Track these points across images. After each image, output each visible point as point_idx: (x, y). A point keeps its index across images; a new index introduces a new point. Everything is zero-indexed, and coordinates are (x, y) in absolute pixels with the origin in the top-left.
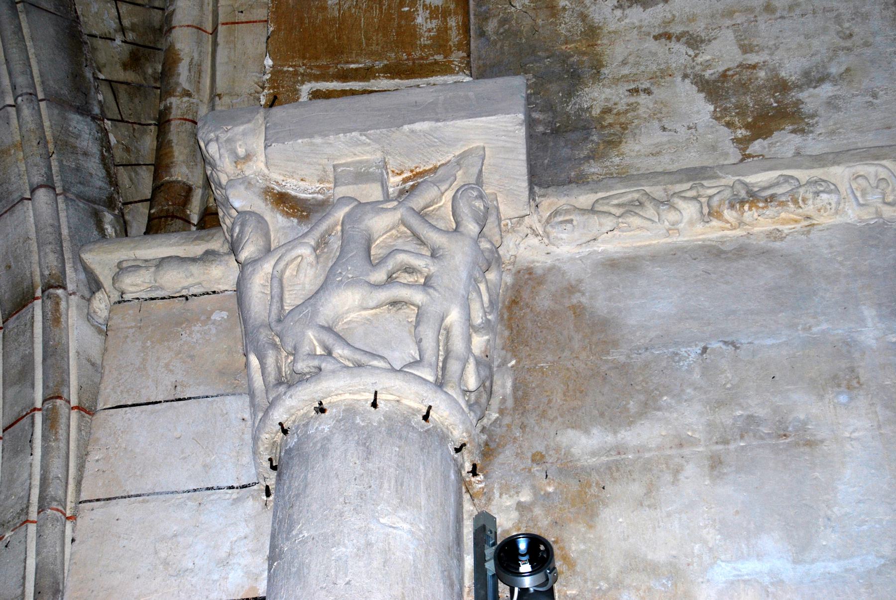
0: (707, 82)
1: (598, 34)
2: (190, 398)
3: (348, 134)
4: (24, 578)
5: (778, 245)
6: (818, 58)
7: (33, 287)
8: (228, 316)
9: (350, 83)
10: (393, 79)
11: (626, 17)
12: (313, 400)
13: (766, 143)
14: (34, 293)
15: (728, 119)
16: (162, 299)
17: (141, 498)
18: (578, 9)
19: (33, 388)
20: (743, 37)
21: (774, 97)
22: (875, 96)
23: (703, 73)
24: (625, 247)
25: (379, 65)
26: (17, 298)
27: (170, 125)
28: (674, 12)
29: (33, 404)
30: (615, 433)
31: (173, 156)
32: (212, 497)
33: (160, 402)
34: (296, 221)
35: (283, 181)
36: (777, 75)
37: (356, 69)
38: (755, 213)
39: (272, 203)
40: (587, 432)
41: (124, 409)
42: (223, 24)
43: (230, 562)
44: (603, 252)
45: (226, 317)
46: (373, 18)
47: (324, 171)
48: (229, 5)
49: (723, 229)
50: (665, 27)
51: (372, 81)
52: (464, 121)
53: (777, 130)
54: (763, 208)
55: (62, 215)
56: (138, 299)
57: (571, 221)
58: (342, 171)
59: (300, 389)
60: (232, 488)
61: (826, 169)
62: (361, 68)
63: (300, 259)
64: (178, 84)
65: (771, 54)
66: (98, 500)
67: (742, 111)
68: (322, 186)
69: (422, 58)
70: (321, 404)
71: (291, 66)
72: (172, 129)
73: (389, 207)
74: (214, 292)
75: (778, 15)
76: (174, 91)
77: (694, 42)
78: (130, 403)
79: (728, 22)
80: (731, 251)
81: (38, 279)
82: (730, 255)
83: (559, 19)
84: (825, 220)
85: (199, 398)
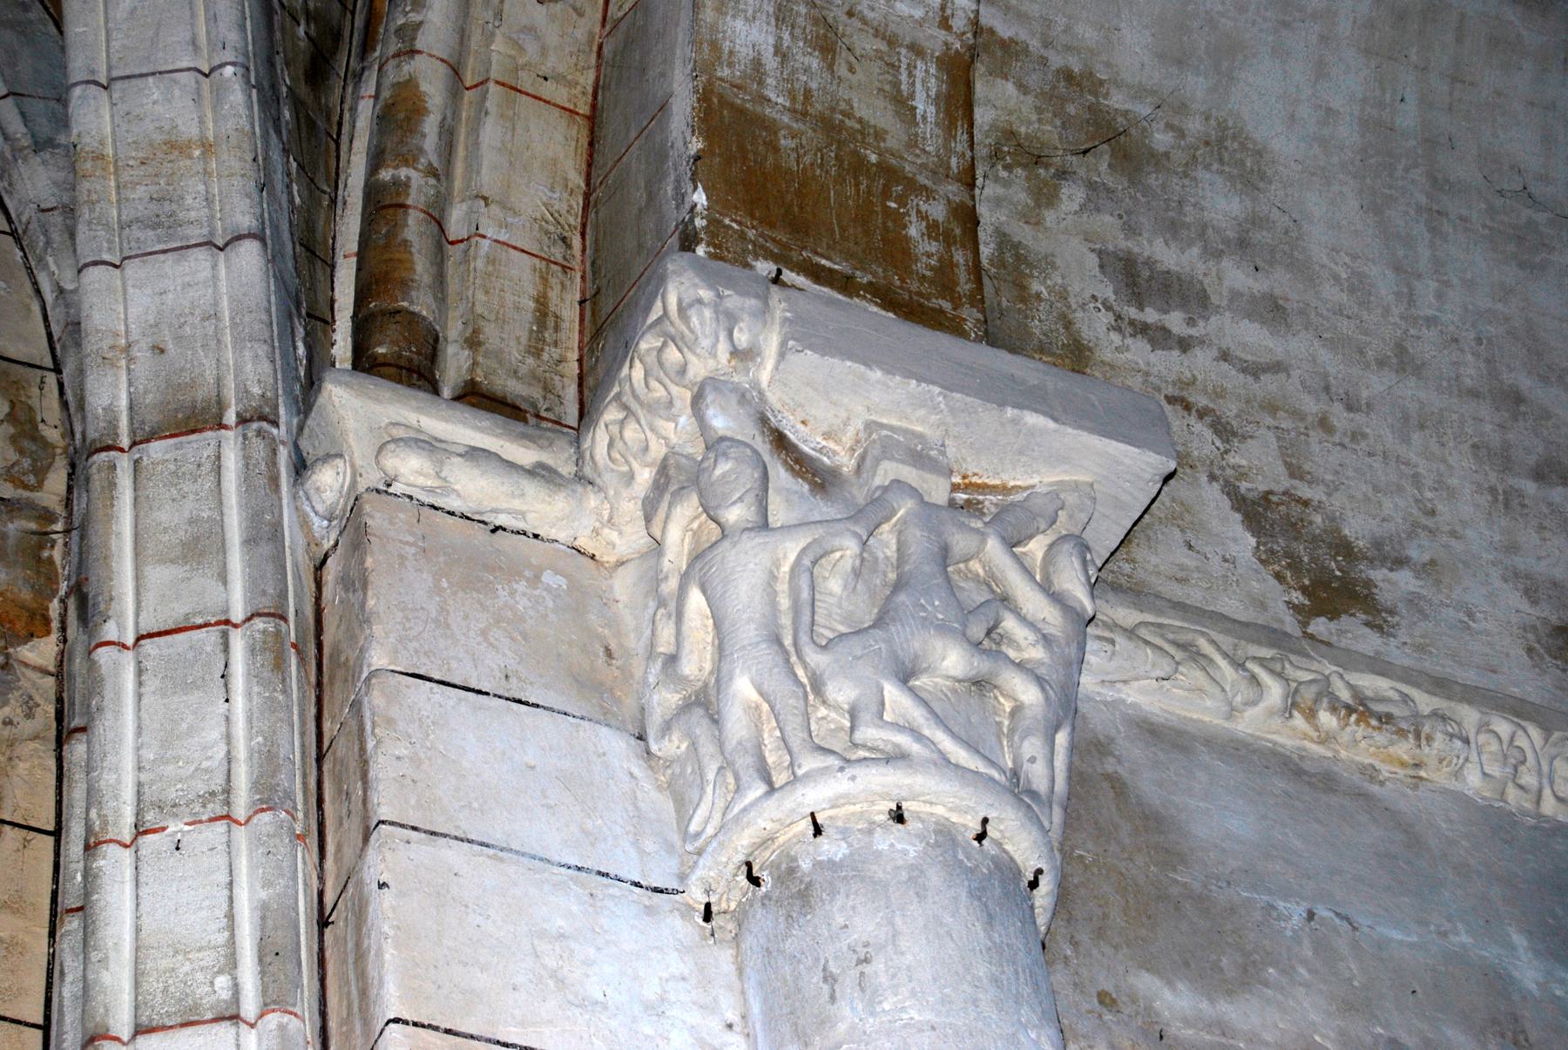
0: (1244, 499)
1: (1088, 358)
3: (923, 385)
4: (231, 916)
5: (1375, 789)
6: (1390, 527)
7: (221, 406)
11: (1128, 349)
12: (885, 796)
13: (1333, 625)
14: (221, 416)
15: (1277, 568)
16: (449, 513)
17: (491, 851)
18: (1059, 305)
19: (225, 583)
20: (1289, 452)
21: (1336, 561)
22: (1471, 615)
23: (1238, 484)
24: (1166, 711)
25: (863, 278)
27: (406, 214)
28: (1195, 372)
29: (226, 611)
30: (1212, 1001)
32: (611, 891)
33: (487, 694)
34: (806, 487)
36: (1338, 530)
37: (831, 270)
38: (1361, 731)
39: (771, 442)
40: (1170, 984)
42: (497, 82)
43: (668, 1013)
44: (1133, 705)
46: (847, 198)
48: (510, 56)
49: (1305, 736)
50: (1182, 389)
52: (1093, 437)
53: (1346, 612)
54: (1374, 728)
56: (411, 497)
57: (1113, 642)
59: (874, 771)
60: (637, 885)
61: (1453, 704)
62: (836, 271)
64: (421, 150)
65: (1329, 495)
66: (414, 828)
67: (1295, 565)
68: (824, 443)
69: (919, 294)
70: (899, 808)
71: (736, 221)
73: (972, 525)
74: (536, 536)
75: (1337, 439)
76: (415, 160)
77: (1223, 430)
78: (437, 677)
79: (1269, 421)
80: (1314, 775)
81: (230, 394)
82: (1314, 780)
83: (1031, 310)
84: (1439, 777)
85: (552, 710)
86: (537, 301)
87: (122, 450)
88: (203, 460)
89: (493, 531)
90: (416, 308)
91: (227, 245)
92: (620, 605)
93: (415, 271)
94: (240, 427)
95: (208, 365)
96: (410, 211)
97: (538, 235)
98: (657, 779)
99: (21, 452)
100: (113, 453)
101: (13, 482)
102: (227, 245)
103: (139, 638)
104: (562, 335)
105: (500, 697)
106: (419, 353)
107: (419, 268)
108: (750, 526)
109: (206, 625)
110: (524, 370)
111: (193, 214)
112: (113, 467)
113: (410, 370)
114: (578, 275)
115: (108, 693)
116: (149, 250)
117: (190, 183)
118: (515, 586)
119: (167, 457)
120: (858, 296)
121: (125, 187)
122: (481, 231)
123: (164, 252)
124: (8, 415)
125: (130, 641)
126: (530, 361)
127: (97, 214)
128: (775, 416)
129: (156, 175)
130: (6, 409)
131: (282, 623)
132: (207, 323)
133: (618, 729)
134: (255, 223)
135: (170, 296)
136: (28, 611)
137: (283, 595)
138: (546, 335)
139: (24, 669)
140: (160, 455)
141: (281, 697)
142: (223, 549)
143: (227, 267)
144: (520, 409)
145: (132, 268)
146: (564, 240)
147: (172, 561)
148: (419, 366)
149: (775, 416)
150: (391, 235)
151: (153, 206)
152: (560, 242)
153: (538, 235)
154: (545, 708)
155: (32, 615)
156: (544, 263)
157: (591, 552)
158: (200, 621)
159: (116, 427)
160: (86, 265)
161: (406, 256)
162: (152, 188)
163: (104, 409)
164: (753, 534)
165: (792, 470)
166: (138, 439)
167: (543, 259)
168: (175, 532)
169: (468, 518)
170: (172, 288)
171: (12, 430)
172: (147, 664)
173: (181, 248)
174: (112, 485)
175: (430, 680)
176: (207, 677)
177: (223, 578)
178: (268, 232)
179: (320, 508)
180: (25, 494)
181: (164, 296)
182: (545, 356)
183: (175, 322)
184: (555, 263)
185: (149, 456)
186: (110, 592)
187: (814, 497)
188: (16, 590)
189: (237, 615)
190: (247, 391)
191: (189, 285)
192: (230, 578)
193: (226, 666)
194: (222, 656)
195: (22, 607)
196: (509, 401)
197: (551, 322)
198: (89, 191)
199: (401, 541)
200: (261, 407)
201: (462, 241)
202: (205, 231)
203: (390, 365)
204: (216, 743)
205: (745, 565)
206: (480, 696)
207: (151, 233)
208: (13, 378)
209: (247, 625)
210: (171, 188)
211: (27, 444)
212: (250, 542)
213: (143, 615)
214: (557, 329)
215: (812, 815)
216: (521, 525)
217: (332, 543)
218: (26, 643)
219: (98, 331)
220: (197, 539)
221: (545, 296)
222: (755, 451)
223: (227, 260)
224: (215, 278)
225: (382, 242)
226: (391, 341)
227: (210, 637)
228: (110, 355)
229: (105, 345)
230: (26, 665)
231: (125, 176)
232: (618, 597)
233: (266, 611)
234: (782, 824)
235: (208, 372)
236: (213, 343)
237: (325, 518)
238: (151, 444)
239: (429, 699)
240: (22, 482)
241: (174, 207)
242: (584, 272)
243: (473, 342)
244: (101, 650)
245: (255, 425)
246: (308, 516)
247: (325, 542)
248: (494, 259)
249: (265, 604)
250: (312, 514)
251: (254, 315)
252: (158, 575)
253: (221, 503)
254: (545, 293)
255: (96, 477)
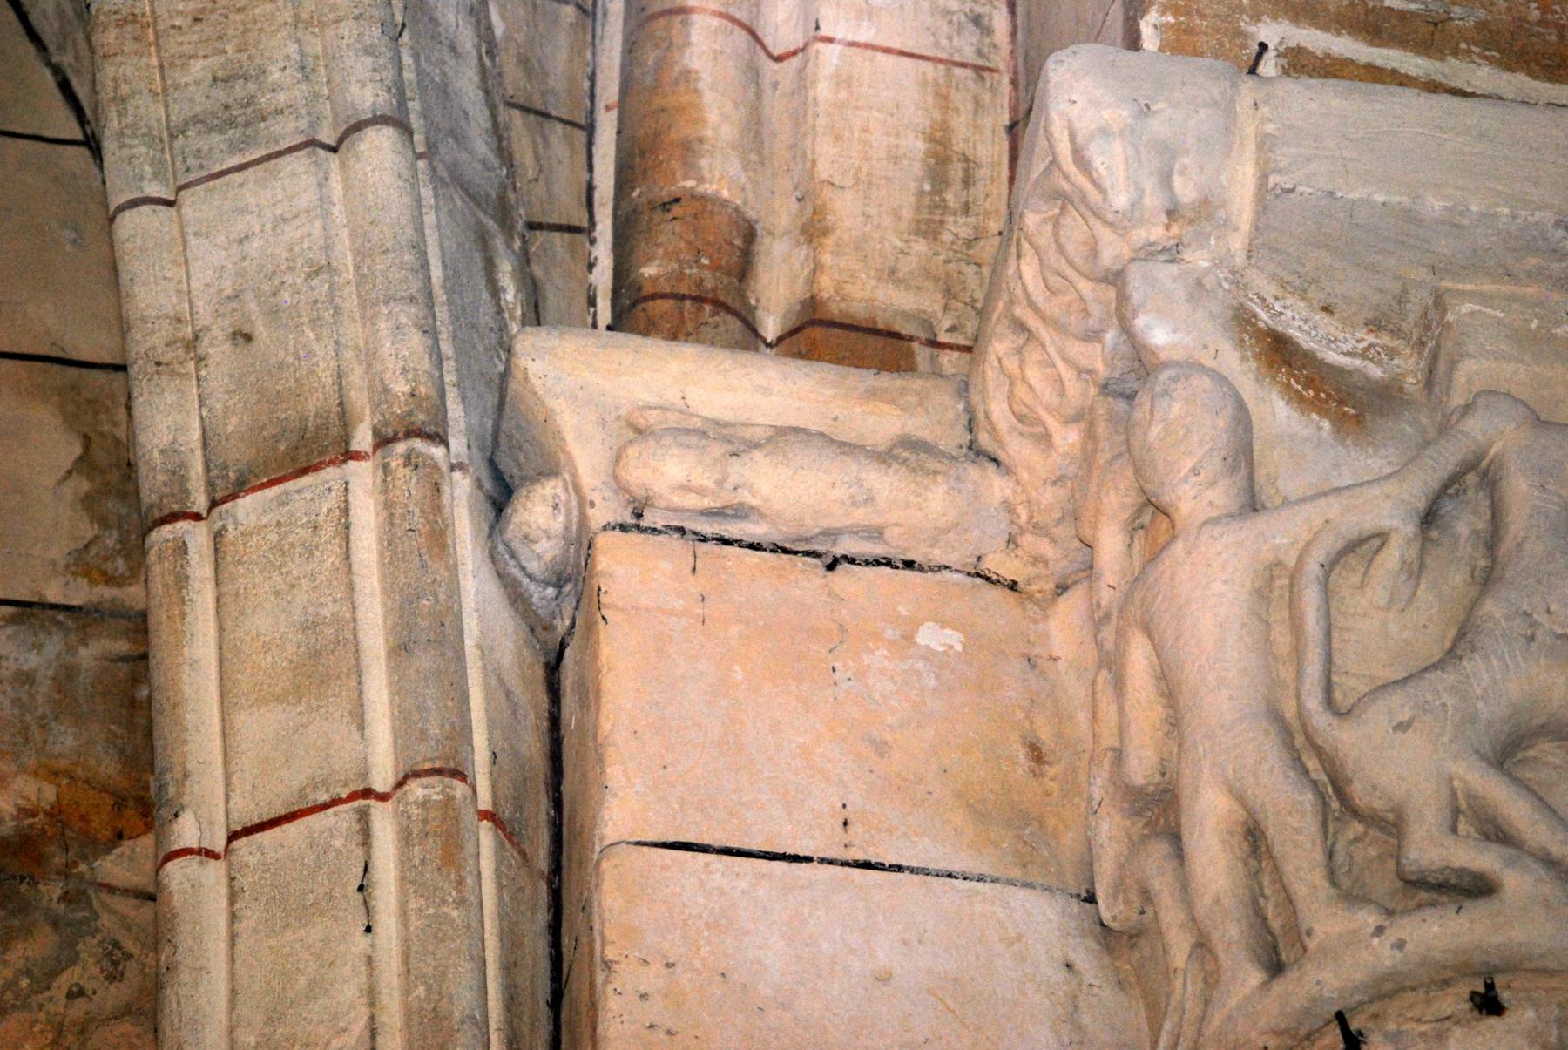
2: (899, 869)
7: (346, 420)
8: (964, 646)
9: (1385, 51)
10: (1510, 68)
16: (751, 546)
19: (362, 727)
26: (276, 438)
29: (364, 775)
31: (702, 121)
33: (808, 859)
34: (1326, 424)
35: (1276, 298)
39: (1257, 357)
41: (701, 857)
45: (959, 647)
47: (1401, 299)
51: (1451, 60)
55: (430, 219)
58: (1472, 313)
63: (1376, 542)
70: (1490, 987)
72: (694, 38)
74: (909, 565)
81: (359, 399)
85: (925, 872)
86: (932, 139)
87: (197, 517)
88: (321, 518)
89: (831, 567)
90: (708, 188)
91: (341, 140)
92: (1061, 665)
93: (703, 121)
94: (379, 453)
95: (321, 354)
96: (695, 17)
97: (929, 21)
98: (1117, 970)
99: (103, 522)
100: (182, 525)
101: (87, 575)
102: (341, 140)
103: (233, 837)
104: (978, 191)
105: (831, 862)
106: (715, 267)
107: (713, 116)
108: (1215, 513)
109: (335, 802)
110: (907, 266)
111: (282, 98)
112: (183, 549)
113: (699, 300)
114: (1006, 80)
115: (184, 940)
116: (217, 168)
117: (274, 43)
118: (866, 659)
119: (265, 520)
120: (1455, 53)
121: (172, 64)
122: (825, 31)
123: (241, 168)
124: (81, 459)
125: (219, 844)
126: (920, 246)
127: (130, 119)
128: (1268, 307)
129: (220, 38)
130: (77, 450)
131: (456, 783)
132: (316, 281)
133: (1048, 889)
134: (383, 97)
135: (256, 243)
136: (113, 794)
137: (463, 732)
138: (949, 196)
139: (105, 897)
140: (253, 518)
141: (455, 914)
142: (358, 671)
143: (345, 181)
144: (897, 336)
145: (195, 205)
146: (977, 20)
147: (279, 699)
148: (714, 290)
149: (1268, 307)
150: (662, 65)
151: (220, 94)
152: (971, 26)
153: (929, 21)
154: (912, 870)
155: (120, 803)
156: (941, 67)
157: (1010, 577)
158: (323, 797)
159: (183, 480)
160: (121, 209)
161: (684, 99)
162: (215, 61)
163: (162, 452)
164: (1219, 529)
165: (1301, 399)
166: (219, 495)
167: (940, 61)
168: (281, 647)
169: (785, 551)
170: (257, 229)
171: (86, 486)
172: (244, 881)
173: (268, 158)
174: (182, 580)
175: (704, 849)
176: (338, 891)
177: (359, 720)
178: (414, 106)
179: (534, 567)
180: (107, 593)
181: (246, 245)
182: (947, 237)
183: (266, 288)
184: (963, 65)
185: (236, 522)
186: (183, 765)
187: (1342, 443)
188: (92, 762)
189: (382, 780)
190: (386, 391)
191: (284, 220)
192: (369, 717)
193: (366, 870)
194: (359, 852)
195: (104, 789)
196: (880, 326)
197: (956, 172)
198: (115, 80)
199: (661, 610)
200: (410, 414)
201: (795, 53)
202: (303, 123)
203: (663, 296)
204: (352, 1006)
205: (1207, 586)
206: (795, 866)
207: (217, 138)
208: (87, 394)
209: (399, 793)
210: (244, 56)
211: (112, 505)
212: (401, 649)
213: (236, 798)
214: (967, 182)
215: (1340, 1017)
216: (878, 550)
217: (567, 622)
218: (109, 851)
219: (144, 319)
220: (315, 655)
221: (944, 127)
222: (1220, 378)
223: (344, 166)
224: (324, 201)
225: (649, 80)
226: (666, 253)
227: (341, 820)
228: (169, 356)
229: (158, 340)
230: (110, 889)
231: (172, 46)
232: (1056, 652)
233: (428, 766)
234: (1294, 1037)
235: (322, 365)
236: (327, 315)
237: (547, 583)
238: (240, 501)
239: (702, 884)
240: (104, 573)
241: (252, 87)
242: (1015, 73)
243: (813, 230)
244: (170, 866)
245: (401, 448)
246: (520, 584)
247: (557, 622)
248: (850, 78)
249: (426, 755)
250: (526, 581)
251: (390, 256)
252: (257, 725)
253: (351, 587)
254: (944, 121)
255: (157, 569)
